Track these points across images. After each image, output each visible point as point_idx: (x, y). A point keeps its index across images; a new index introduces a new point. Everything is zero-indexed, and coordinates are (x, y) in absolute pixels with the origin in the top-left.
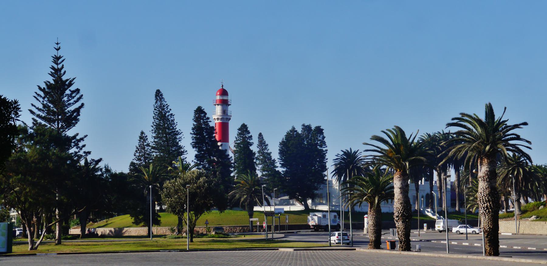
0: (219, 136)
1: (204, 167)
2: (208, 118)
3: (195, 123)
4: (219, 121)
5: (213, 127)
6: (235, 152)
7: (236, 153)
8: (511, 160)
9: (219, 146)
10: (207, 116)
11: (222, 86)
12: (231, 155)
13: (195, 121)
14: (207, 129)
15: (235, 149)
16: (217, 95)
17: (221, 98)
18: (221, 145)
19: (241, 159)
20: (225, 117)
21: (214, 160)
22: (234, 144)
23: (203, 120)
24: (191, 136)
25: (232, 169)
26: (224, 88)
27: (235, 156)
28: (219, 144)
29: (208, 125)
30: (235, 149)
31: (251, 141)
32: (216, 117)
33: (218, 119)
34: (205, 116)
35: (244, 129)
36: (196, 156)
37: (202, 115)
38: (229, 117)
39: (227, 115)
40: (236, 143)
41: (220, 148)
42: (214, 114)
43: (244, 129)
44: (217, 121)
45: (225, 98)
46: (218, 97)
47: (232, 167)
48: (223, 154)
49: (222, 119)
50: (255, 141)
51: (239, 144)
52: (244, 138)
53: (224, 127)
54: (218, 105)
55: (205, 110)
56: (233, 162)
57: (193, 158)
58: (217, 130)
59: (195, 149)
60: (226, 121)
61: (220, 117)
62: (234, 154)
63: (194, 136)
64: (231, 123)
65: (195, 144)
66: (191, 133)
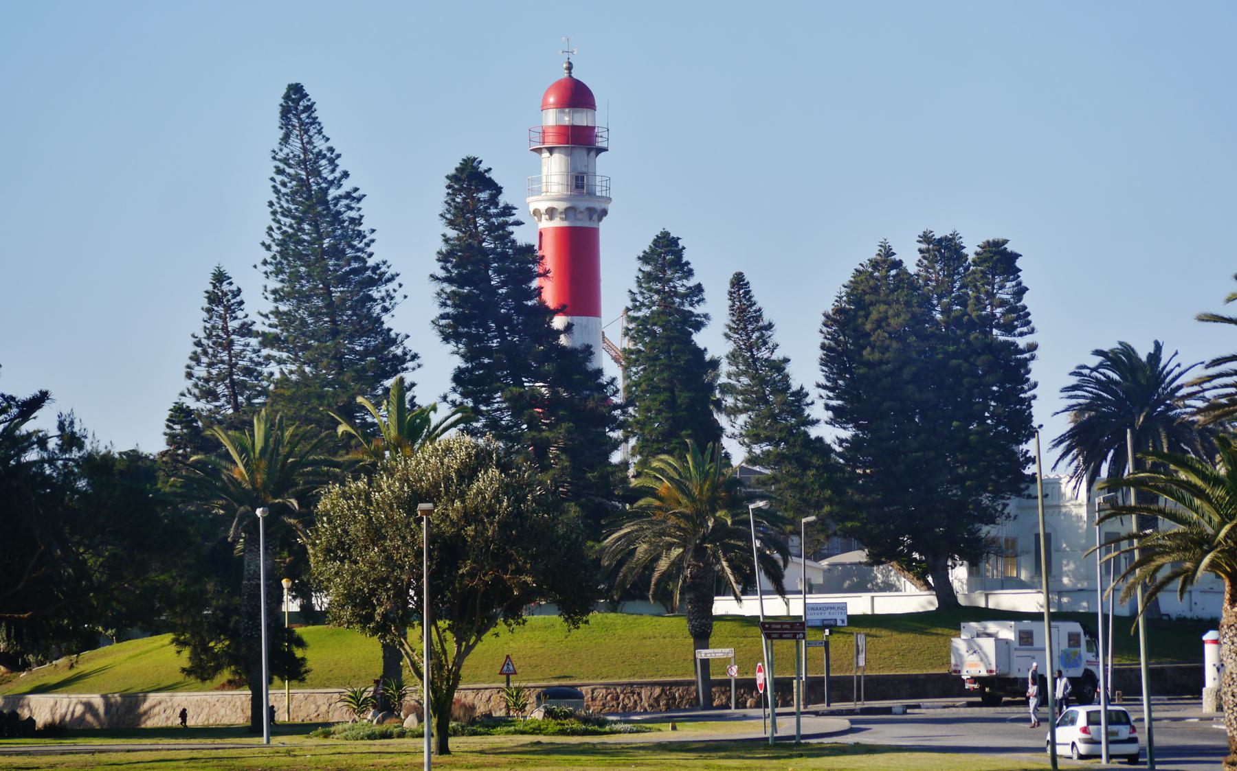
1: (493, 424)
2: (508, 210)
3: (452, 233)
4: (558, 222)
5: (529, 249)
6: (627, 359)
7: (635, 363)
9: (558, 332)
10: (503, 200)
11: (570, 68)
12: (611, 369)
13: (451, 223)
15: (627, 344)
16: (544, 107)
17: (566, 120)
18: (569, 328)
19: (654, 389)
20: (583, 204)
22: (622, 323)
23: (488, 217)
24: (436, 287)
25: (617, 434)
28: (559, 322)
30: (627, 344)
31: (698, 310)
32: (543, 206)
33: (551, 212)
34: (493, 201)
35: (666, 256)
36: (460, 378)
37: (484, 195)
38: (598, 206)
39: (591, 194)
41: (563, 340)
42: (533, 192)
43: (666, 256)
44: (545, 224)
45: (581, 119)
46: (552, 118)
48: (575, 367)
49: (569, 212)
50: (716, 308)
51: (645, 320)
53: (580, 247)
58: (550, 263)
59: (451, 346)
61: (561, 206)
62: (626, 369)
63: (449, 288)
65: (454, 327)
66: (434, 277)
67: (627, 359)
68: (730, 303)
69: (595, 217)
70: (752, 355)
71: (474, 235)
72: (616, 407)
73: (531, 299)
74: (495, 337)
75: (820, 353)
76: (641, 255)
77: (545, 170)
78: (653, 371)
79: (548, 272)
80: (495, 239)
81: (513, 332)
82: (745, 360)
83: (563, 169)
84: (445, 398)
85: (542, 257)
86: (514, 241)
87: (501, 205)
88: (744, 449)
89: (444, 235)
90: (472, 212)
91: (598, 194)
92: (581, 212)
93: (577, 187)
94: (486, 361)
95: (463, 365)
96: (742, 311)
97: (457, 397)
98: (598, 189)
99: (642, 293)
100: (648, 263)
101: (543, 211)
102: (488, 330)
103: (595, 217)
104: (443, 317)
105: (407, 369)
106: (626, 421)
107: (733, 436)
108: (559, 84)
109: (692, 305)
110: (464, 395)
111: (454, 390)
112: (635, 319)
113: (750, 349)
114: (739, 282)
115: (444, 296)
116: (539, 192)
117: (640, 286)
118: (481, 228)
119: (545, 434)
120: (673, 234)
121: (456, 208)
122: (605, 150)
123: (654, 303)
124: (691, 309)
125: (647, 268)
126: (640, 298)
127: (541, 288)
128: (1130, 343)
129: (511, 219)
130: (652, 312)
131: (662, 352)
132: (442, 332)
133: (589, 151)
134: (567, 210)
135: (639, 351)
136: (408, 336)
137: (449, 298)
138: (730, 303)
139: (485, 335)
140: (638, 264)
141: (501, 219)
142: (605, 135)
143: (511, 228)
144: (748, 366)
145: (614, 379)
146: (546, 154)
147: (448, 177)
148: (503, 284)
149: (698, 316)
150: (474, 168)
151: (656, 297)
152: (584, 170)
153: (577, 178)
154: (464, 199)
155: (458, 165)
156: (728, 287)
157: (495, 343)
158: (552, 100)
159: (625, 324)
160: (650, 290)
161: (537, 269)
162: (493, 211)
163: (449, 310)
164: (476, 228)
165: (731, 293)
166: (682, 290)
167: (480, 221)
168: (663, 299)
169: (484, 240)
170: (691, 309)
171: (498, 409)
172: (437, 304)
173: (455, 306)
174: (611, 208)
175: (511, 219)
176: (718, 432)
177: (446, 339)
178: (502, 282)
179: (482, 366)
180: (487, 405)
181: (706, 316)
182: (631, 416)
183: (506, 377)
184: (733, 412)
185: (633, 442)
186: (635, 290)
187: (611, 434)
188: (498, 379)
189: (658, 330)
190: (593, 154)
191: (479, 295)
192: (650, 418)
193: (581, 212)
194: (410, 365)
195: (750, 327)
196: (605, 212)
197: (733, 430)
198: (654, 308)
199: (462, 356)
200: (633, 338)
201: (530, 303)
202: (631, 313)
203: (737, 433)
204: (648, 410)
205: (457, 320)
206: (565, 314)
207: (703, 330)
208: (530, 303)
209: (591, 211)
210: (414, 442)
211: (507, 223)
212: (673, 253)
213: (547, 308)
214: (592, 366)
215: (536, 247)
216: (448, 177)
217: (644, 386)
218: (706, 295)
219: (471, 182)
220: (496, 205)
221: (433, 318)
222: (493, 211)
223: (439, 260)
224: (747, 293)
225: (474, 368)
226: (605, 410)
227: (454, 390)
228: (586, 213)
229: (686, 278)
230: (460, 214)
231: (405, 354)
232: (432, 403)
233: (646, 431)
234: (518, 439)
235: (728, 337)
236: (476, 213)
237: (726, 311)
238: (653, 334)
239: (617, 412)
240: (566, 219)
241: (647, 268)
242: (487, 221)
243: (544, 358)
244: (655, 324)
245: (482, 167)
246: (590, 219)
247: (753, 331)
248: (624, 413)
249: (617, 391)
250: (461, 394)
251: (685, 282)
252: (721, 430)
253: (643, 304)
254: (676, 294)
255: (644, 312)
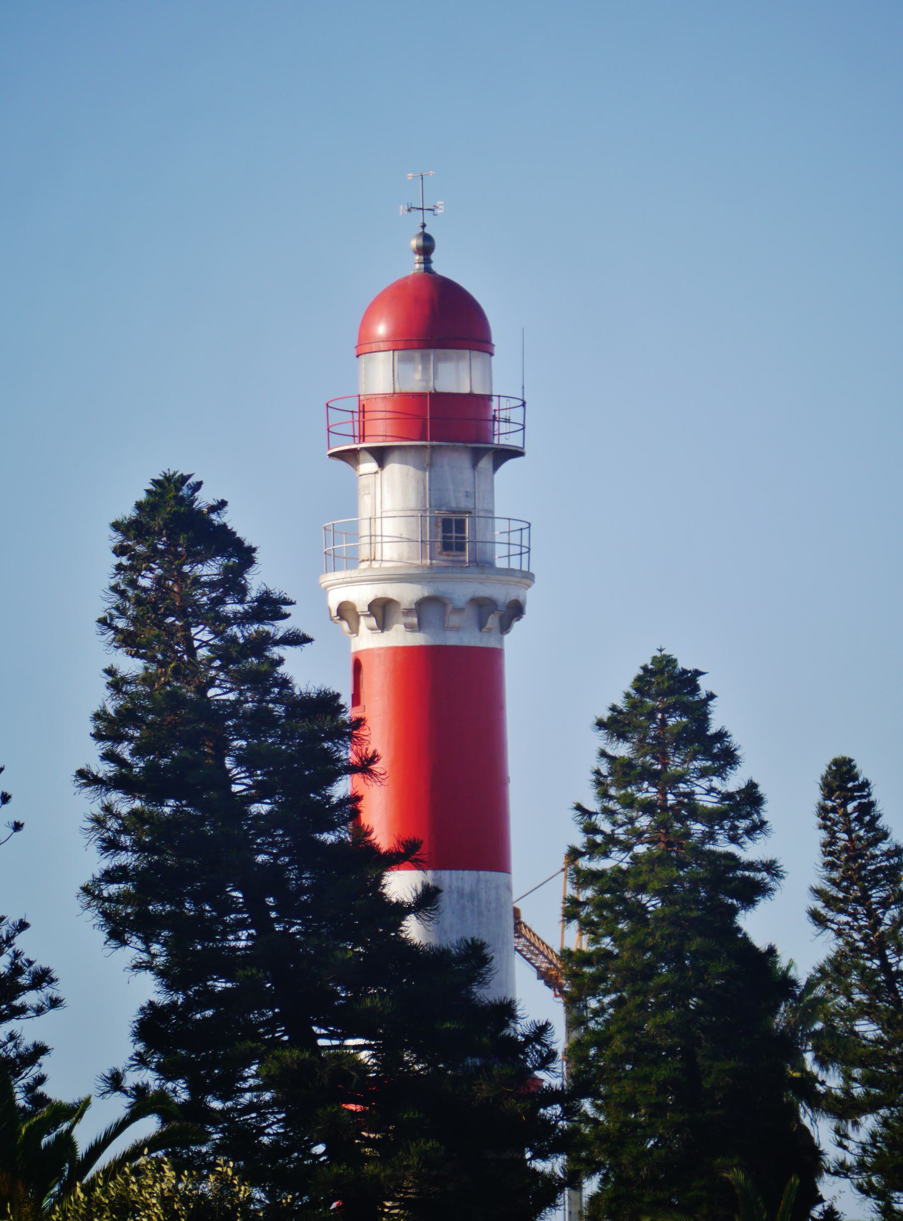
0: (407, 804)
1: (240, 1141)
2: (270, 607)
3: (131, 666)
4: (400, 636)
5: (327, 703)
6: (571, 976)
7: (593, 987)
8: (889, 1046)
9: (400, 911)
10: (257, 581)
11: (426, 248)
12: (537, 1004)
13: (128, 641)
14: (258, 722)
15: (574, 939)
16: (364, 346)
17: (415, 380)
18: (427, 900)
19: (643, 1052)
20: (463, 590)
21: (344, 1064)
22: (561, 888)
23: (218, 623)
24: (91, 803)
25: (554, 1166)
26: (442, 266)
27: (575, 1023)
28: (400, 885)
29: (265, 679)
30: (574, 939)
31: (751, 851)
32: (362, 595)
33: (382, 611)
34: (231, 583)
35: (667, 713)
36: (152, 1027)
37: (210, 570)
38: (501, 593)
39: (483, 564)
40: (584, 878)
41: (414, 929)
43: (667, 713)
44: (368, 640)
45: (456, 375)
46: (383, 375)
47: (550, 1142)
48: (447, 995)
49: (426, 610)
51: (614, 882)
52: (673, 816)
53: (455, 697)
54: (381, 455)
55: (230, 518)
56: (553, 1078)
57: (122, 1048)
58: (379, 737)
59: (133, 952)
60: (470, 638)
61: (406, 594)
62: (573, 1002)
63: (124, 805)
64: (521, 654)
65: (138, 899)
66: (86, 777)
67: (574, 976)
68: (823, 835)
69: (493, 621)
70: (885, 966)
71: (188, 670)
72: (551, 1096)
73: (331, 827)
74: (241, 925)
75: (778, 953)
76: (605, 715)
77: (366, 505)
78: (643, 1006)
79: (374, 758)
80: (239, 679)
81: (287, 911)
82: (867, 977)
83: (413, 502)
84: (115, 1082)
85: (359, 723)
86: (285, 683)
87: (253, 594)
88: (871, 1203)
89: (110, 672)
90: (181, 613)
91: (500, 563)
92: (458, 610)
93: (447, 546)
94: (221, 985)
95: (162, 999)
96: (855, 852)
97: (149, 1078)
98: (500, 551)
99: (609, 813)
100: (622, 736)
101: (362, 607)
102: (228, 906)
103: (493, 621)
104: (110, 876)
105: (21, 1011)
106: (575, 1131)
107: (842, 1170)
108: (399, 290)
109: (734, 839)
110: (166, 1072)
111: (141, 1061)
112: (584, 878)
113: (877, 949)
114: (842, 781)
115: (113, 824)
116: (352, 560)
117: (604, 795)
118: (203, 653)
119: (369, 1168)
120: (685, 663)
121: (139, 602)
122: (517, 453)
123: (639, 835)
124: (732, 848)
125: (622, 750)
126: (606, 826)
127: (355, 799)
128: (287, 620)
129: (280, 628)
130: (635, 858)
131: (661, 957)
132: (104, 913)
133: (476, 456)
134: (422, 605)
135: (606, 955)
136: (23, 926)
137: (124, 830)
138: (823, 835)
139: (219, 920)
140: (599, 740)
141: (253, 628)
142: (516, 415)
143: (276, 652)
144: (875, 993)
145: (542, 1029)
146: (368, 466)
147: (116, 526)
148: (261, 792)
149: (750, 866)
150: (180, 500)
151: (644, 822)
152: (464, 503)
153: (446, 524)
154: (158, 580)
155: (142, 497)
156: (816, 795)
157: (242, 941)
158: (381, 329)
159: (571, 891)
160: (629, 803)
161: (349, 755)
162: (231, 608)
163: (125, 859)
164: (192, 651)
165: (824, 812)
166: (709, 802)
167: (202, 634)
168: (663, 825)
169: (211, 684)
170: (732, 848)
171: (250, 1107)
172: (94, 849)
173: (139, 847)
174: (533, 599)
175: (280, 628)
176: (810, 1159)
177: (117, 936)
178: (257, 785)
179: (208, 998)
180: (224, 1098)
181: (770, 867)
182: (586, 1119)
183: (271, 1025)
184: (845, 1109)
185: (591, 1186)
186: (593, 805)
187: (540, 1165)
188: (251, 1031)
189: (651, 902)
190: (485, 463)
191: (200, 821)
192: (636, 1125)
193: (458, 610)
194: (30, 998)
195: (876, 895)
196: (516, 610)
197: (840, 1154)
198: (640, 849)
199: (161, 973)
200: (587, 926)
201: (329, 838)
202: (584, 863)
203: (851, 1160)
204: (631, 1105)
205: (146, 883)
206: (419, 865)
207: (763, 905)
208: (329, 838)
209: (482, 607)
210: (42, 1193)
211: (266, 640)
212: (685, 709)
213: (373, 849)
214: (487, 994)
215: (346, 699)
216: (116, 526)
217: (618, 1045)
218: (768, 812)
219: (175, 530)
220: (241, 591)
221: (86, 879)
222: (231, 608)
223: (98, 736)
224: (866, 808)
225: (191, 1005)
226: (519, 1107)
227: (141, 1061)
228: (471, 613)
229: (719, 772)
230: (147, 620)
231: (16, 970)
232: (83, 1096)
233: (625, 1159)
234: (303, 1178)
235: (818, 918)
236: (192, 614)
237: (817, 857)
238: (637, 913)
239: (553, 1111)
240: (419, 627)
241: (622, 750)
242: (217, 633)
243: (359, 976)
244: (641, 889)
245: (204, 499)
246: (481, 625)
247: (885, 904)
248: (570, 1112)
249: (552, 1055)
250: (159, 1069)
251: (716, 782)
252: (816, 1153)
253: (611, 839)
254: (695, 812)
255: (618, 860)
